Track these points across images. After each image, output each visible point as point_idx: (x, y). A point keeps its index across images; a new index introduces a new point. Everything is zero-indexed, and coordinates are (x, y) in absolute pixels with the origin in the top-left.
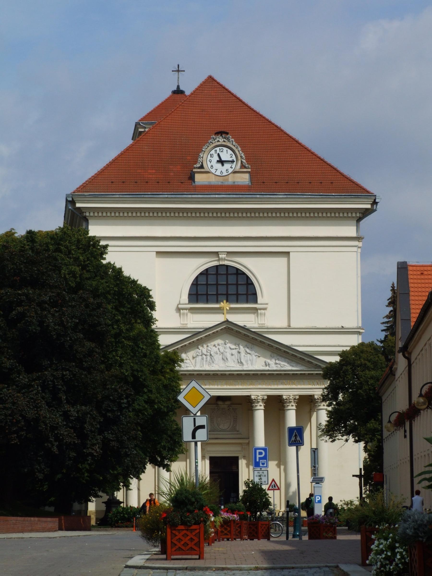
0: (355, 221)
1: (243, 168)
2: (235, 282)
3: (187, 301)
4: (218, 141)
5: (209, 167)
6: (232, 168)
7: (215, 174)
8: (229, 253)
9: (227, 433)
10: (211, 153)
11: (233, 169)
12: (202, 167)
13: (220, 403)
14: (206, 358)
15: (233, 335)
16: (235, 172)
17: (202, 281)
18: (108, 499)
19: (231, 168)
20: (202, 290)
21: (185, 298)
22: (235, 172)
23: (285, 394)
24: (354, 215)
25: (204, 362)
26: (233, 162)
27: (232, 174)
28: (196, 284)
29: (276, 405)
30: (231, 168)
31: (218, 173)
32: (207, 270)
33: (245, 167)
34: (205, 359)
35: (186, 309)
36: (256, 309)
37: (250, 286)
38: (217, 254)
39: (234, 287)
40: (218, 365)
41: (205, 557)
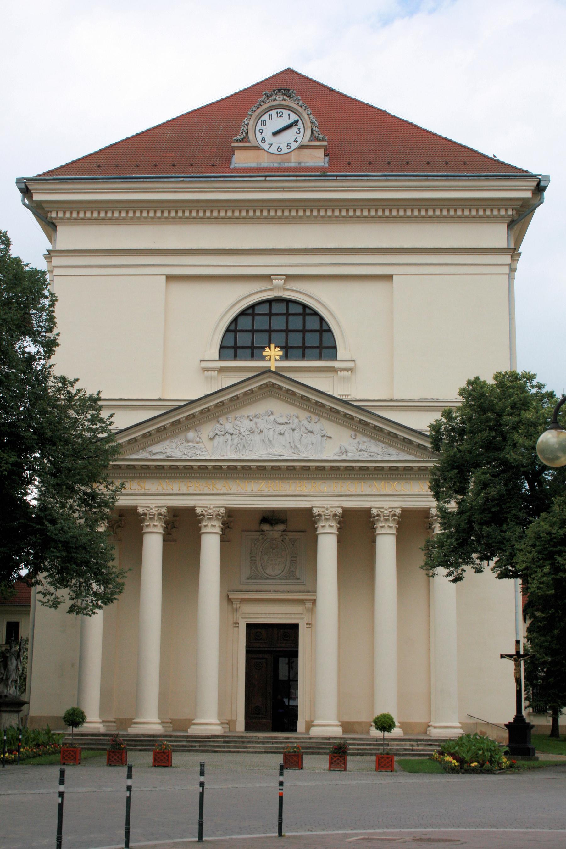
0: (506, 226)
3: (216, 357)
4: (275, 100)
5: (259, 140)
6: (297, 141)
8: (289, 277)
9: (278, 581)
10: (262, 119)
11: (298, 143)
12: (245, 139)
13: (266, 527)
14: (232, 440)
19: (296, 141)
23: (375, 505)
24: (503, 212)
25: (229, 447)
26: (296, 122)
27: (296, 151)
28: (233, 329)
29: (357, 528)
31: (274, 150)
32: (252, 307)
33: (318, 139)
34: (229, 442)
36: (333, 370)
37: (325, 335)
38: (268, 278)
39: (291, 335)
40: (257, 452)
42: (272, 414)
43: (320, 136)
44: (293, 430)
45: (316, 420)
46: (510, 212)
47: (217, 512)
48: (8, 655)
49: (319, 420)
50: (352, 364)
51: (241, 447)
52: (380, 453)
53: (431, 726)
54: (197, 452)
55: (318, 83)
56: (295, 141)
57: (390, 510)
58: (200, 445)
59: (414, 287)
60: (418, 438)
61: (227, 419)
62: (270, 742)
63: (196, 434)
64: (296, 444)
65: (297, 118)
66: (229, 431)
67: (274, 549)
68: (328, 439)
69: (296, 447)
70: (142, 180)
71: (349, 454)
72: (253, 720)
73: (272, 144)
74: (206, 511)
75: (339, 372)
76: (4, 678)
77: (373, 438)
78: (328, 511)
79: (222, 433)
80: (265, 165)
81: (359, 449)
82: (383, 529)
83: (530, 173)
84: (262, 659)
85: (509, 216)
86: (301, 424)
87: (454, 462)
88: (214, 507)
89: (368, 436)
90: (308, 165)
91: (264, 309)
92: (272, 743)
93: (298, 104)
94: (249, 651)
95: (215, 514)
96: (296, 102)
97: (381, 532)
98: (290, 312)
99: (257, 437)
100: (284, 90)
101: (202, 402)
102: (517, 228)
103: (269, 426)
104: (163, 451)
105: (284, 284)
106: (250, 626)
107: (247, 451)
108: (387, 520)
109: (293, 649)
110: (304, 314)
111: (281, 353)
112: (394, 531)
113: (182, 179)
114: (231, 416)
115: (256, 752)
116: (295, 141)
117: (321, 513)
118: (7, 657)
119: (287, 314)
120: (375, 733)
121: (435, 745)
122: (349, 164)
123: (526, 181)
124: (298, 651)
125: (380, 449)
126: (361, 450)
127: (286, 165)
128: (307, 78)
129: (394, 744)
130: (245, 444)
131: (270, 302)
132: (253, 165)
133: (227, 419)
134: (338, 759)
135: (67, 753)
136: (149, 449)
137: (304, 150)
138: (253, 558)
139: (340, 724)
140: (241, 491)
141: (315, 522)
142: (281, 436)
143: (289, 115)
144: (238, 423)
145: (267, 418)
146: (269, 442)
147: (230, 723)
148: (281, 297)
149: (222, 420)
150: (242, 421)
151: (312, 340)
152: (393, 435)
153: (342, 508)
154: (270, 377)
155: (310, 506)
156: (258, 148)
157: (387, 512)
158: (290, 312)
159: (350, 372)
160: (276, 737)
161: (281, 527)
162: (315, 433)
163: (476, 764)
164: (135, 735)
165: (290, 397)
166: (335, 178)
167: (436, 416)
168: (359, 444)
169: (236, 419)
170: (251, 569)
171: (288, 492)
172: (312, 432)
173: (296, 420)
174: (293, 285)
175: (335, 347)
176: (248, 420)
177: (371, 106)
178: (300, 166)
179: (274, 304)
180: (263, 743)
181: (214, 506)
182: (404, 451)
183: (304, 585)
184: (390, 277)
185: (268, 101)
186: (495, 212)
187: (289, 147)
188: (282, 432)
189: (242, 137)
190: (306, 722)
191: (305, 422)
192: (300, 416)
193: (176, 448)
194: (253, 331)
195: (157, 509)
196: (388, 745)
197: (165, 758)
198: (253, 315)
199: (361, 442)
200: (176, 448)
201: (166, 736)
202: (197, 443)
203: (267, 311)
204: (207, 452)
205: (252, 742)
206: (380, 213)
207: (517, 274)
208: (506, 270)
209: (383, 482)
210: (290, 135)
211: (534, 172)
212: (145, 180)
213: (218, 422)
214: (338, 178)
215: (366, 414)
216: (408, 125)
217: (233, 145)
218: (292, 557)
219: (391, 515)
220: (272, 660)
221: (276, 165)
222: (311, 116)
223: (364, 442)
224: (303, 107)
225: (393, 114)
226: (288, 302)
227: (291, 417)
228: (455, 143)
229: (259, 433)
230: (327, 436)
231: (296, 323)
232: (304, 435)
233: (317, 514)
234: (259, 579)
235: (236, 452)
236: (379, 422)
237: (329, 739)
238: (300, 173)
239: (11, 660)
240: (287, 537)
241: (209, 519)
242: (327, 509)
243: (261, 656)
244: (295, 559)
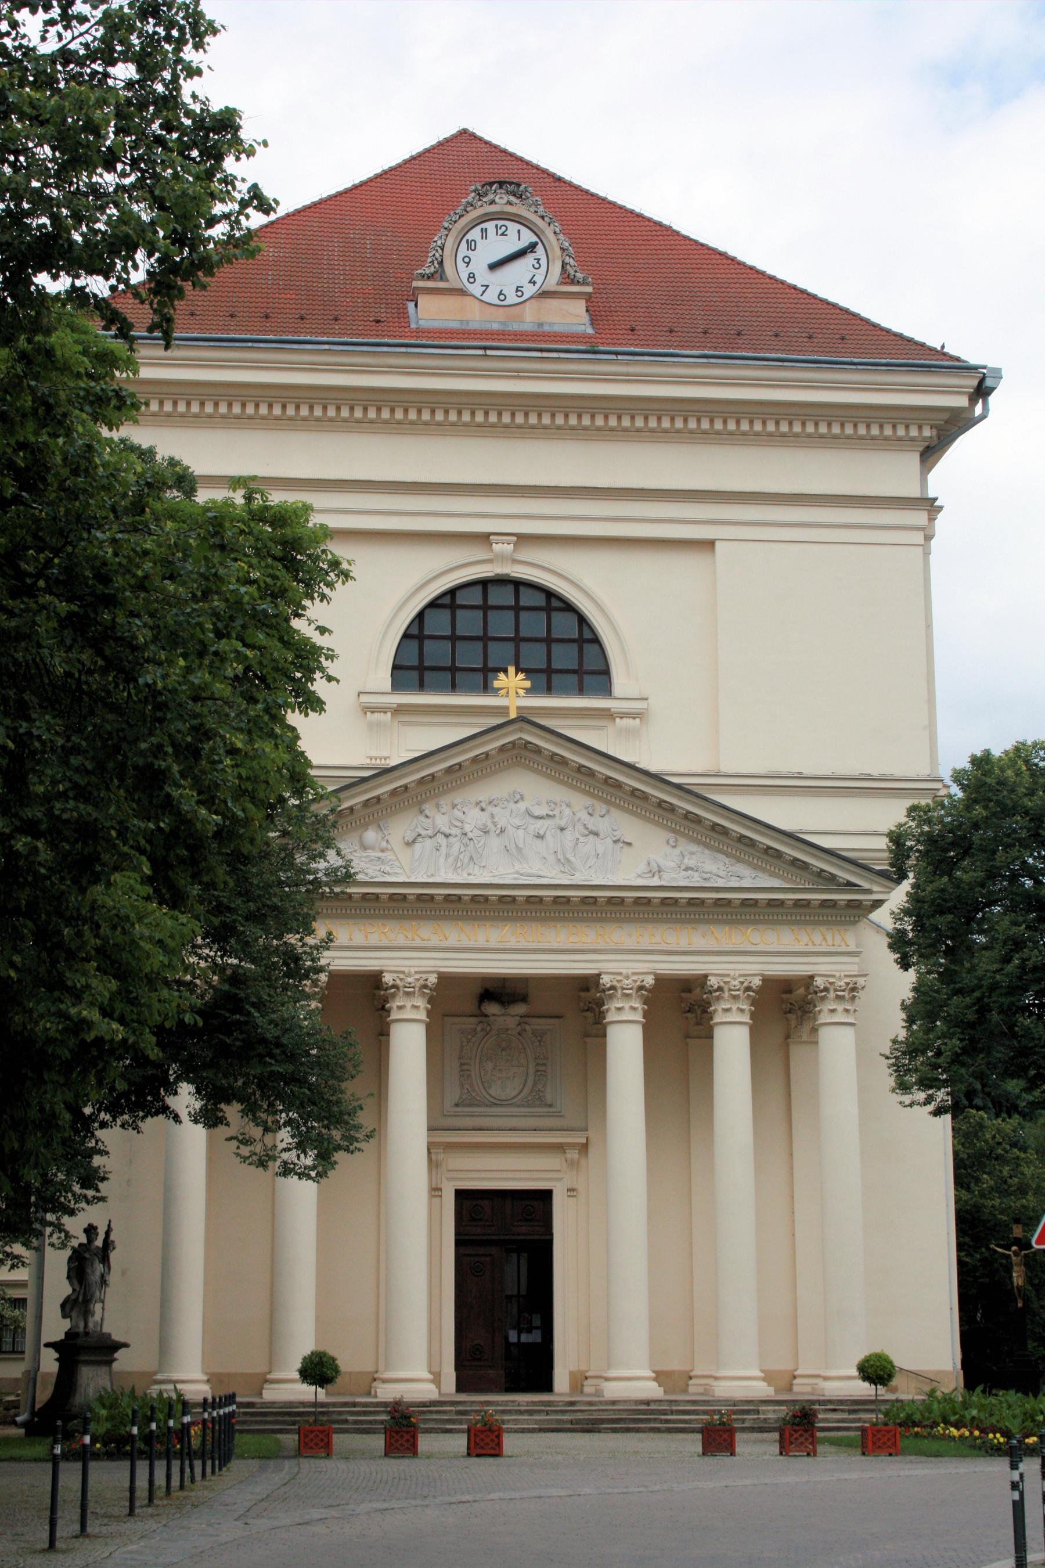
0: (916, 457)
1: (565, 284)
2: (542, 648)
3: (387, 684)
5: (464, 277)
6: (534, 283)
7: (482, 298)
8: (523, 539)
9: (514, 1109)
10: (469, 237)
11: (538, 286)
12: (439, 274)
13: (492, 1009)
15: (540, 773)
16: (544, 294)
17: (439, 623)
18: (68, 1334)
20: (437, 653)
21: (383, 678)
22: (544, 294)
25: (442, 860)
26: (532, 247)
27: (533, 301)
28: (415, 634)
29: (681, 1011)
31: (491, 296)
32: (452, 592)
33: (573, 282)
34: (443, 849)
35: (383, 710)
36: (608, 715)
37: (590, 649)
38: (484, 538)
40: (495, 869)
42: (522, 798)
43: (578, 274)
44: (562, 829)
45: (604, 812)
46: (927, 433)
47: (422, 982)
48: (87, 1255)
49: (608, 811)
51: (466, 860)
52: (722, 873)
53: (380, 1379)
54: (383, 867)
55: (528, 163)
56: (530, 282)
57: (741, 979)
59: (754, 563)
60: (793, 847)
61: (438, 806)
62: (543, 1411)
63: (380, 834)
64: (568, 856)
65: (535, 239)
67: (503, 1049)
68: (626, 848)
69: (568, 860)
70: (250, 344)
71: (665, 876)
73: (487, 286)
74: (401, 980)
75: (618, 720)
76: (80, 1299)
77: (707, 846)
78: (629, 981)
79: (430, 833)
80: (474, 326)
81: (683, 867)
82: (728, 1014)
83: (964, 361)
84: (485, 1255)
85: (924, 439)
86: (576, 818)
87: (945, 900)
88: (416, 972)
89: (699, 842)
90: (556, 328)
91: (474, 597)
92: (547, 1413)
93: (536, 212)
94: (460, 1243)
95: (418, 984)
97: (724, 1020)
99: (495, 843)
100: (511, 183)
101: (397, 773)
103: (517, 822)
105: (515, 550)
106: (461, 1195)
107: (476, 867)
108: (735, 998)
109: (543, 1237)
110: (548, 609)
111: (528, 684)
113: (326, 347)
114: (445, 802)
115: (523, 1431)
116: (530, 282)
117: (615, 983)
118: (86, 1259)
119: (517, 609)
120: (306, 1392)
121: (842, 1410)
122: (633, 330)
123: (958, 376)
125: (722, 868)
126: (687, 869)
127: (515, 327)
128: (505, 152)
129: (768, 1411)
130: (474, 856)
131: (484, 584)
132: (455, 325)
133: (438, 806)
134: (801, 1435)
135: (311, 1436)
137: (548, 300)
138: (465, 1067)
140: (465, 942)
142: (539, 841)
143: (519, 231)
144: (459, 814)
145: (512, 805)
146: (517, 852)
149: (429, 808)
150: (466, 811)
151: (564, 657)
152: (747, 841)
153: (655, 974)
154: (521, 730)
155: (596, 972)
156: (462, 292)
157: (736, 983)
158: (522, 603)
159: (638, 720)
160: (553, 1402)
161: (520, 1009)
162: (602, 835)
163: (1035, 1439)
164: (286, 1403)
165: (557, 768)
166: (614, 357)
167: (892, 814)
168: (683, 857)
169: (454, 806)
170: (462, 1086)
171: (555, 945)
172: (596, 834)
173: (567, 811)
174: (529, 554)
176: (477, 810)
177: (640, 216)
178: (540, 330)
179: (492, 589)
180: (530, 1412)
181: (416, 969)
182: (764, 870)
183: (562, 1116)
185: (480, 203)
186: (901, 432)
187: (519, 294)
188: (542, 833)
189: (432, 269)
190: (571, 1373)
191: (583, 815)
192: (574, 805)
194: (454, 638)
196: (758, 1412)
197: (492, 1440)
198: (453, 607)
199: (686, 853)
202: (382, 851)
203: (479, 602)
204: (402, 867)
205: (510, 1412)
206: (692, 424)
208: (918, 537)
209: (727, 929)
210: (521, 270)
211: (973, 361)
212: (255, 345)
213: (421, 812)
214: (619, 357)
215: (699, 801)
216: (718, 257)
217: (415, 284)
218: (537, 1064)
219: (742, 989)
220: (505, 1256)
221: (495, 326)
222: (561, 236)
223: (692, 853)
224: (546, 219)
225: (684, 232)
226: (518, 584)
227: (556, 804)
228: (814, 297)
229: (498, 835)
230: (624, 842)
232: (582, 839)
233: (608, 986)
234: (479, 1106)
235: (455, 869)
236: (723, 816)
237: (648, 1403)
238: (543, 344)
239: (92, 1264)
240: (527, 1028)
241: (408, 994)
242: (627, 977)
243: (481, 1251)
244: (543, 1068)
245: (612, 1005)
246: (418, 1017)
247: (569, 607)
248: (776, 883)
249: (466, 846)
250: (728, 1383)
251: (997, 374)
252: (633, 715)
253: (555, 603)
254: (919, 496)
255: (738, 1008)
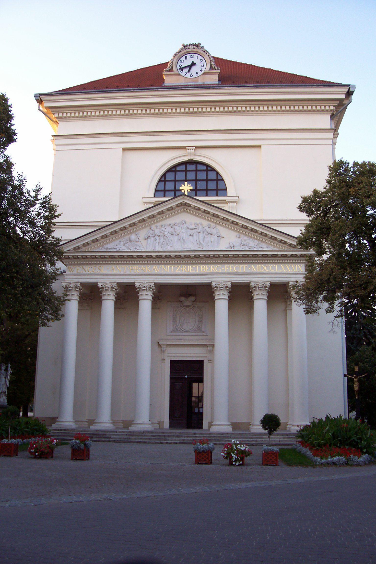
3: (153, 196)
4: (189, 48)
8: (197, 147)
14: (159, 239)
16: (205, 74)
19: (201, 71)
25: (157, 244)
28: (163, 179)
29: (241, 294)
30: (201, 71)
34: (158, 241)
36: (225, 202)
38: (184, 148)
40: (176, 246)
41: (245, 420)
44: (199, 233)
46: (332, 108)
50: (236, 198)
51: (165, 244)
58: (139, 243)
64: (201, 241)
66: (157, 234)
68: (222, 238)
69: (200, 243)
72: (175, 420)
85: (331, 110)
96: (201, 49)
98: (198, 169)
102: (336, 119)
103: (183, 231)
104: (115, 247)
110: (207, 171)
112: (265, 297)
117: (217, 286)
119: (196, 171)
124: (203, 377)
136: (106, 246)
139: (230, 423)
141: (214, 292)
145: (182, 225)
147: (160, 423)
148: (192, 160)
154: (183, 198)
155: (210, 282)
156: (178, 75)
157: (261, 285)
161: (193, 298)
170: (173, 325)
173: (201, 227)
175: (226, 190)
179: (188, 166)
180: (178, 436)
184: (260, 146)
189: (169, 69)
190: (209, 423)
193: (123, 245)
195: (110, 284)
198: (176, 171)
199: (243, 240)
200: (123, 245)
201: (114, 432)
207: (337, 146)
208: (330, 142)
213: (150, 228)
231: (201, 176)
232: (206, 236)
245: (216, 293)
246: (148, 298)
247: (213, 170)
248: (271, 248)
249: (165, 239)
250: (218, 427)
251: (354, 87)
252: (234, 202)
253: (209, 169)
254: (330, 128)
255: (262, 294)
